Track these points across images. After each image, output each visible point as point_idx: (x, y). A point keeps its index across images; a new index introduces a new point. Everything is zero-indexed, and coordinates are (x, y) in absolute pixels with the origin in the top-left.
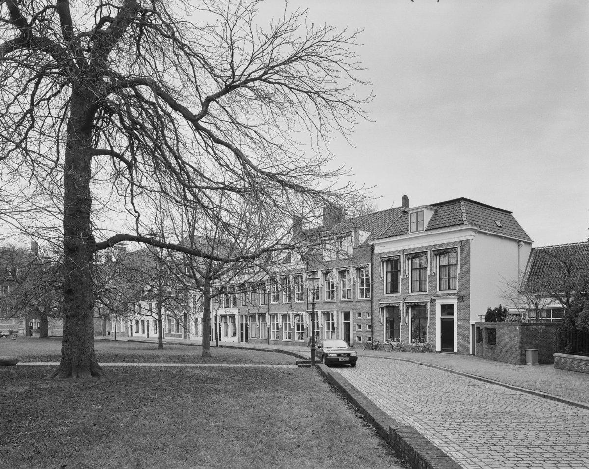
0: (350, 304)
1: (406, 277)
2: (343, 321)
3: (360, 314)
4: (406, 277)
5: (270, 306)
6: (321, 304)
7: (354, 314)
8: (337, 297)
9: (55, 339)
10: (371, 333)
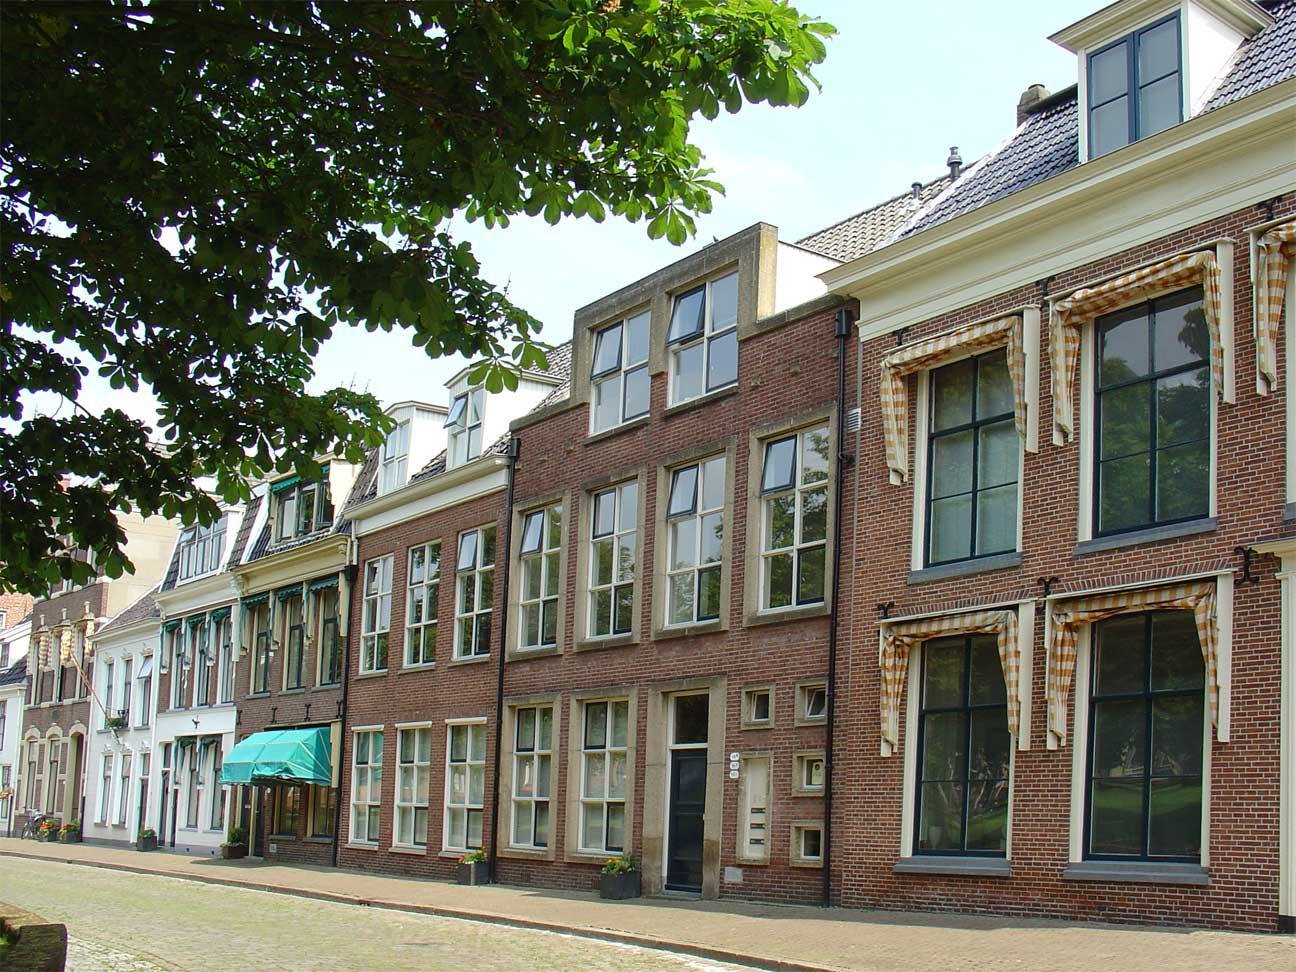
1: (1057, 440)
2: (671, 745)
3: (763, 701)
4: (1057, 440)
5: (352, 688)
6: (563, 662)
7: (733, 703)
8: (647, 617)
10: (821, 808)
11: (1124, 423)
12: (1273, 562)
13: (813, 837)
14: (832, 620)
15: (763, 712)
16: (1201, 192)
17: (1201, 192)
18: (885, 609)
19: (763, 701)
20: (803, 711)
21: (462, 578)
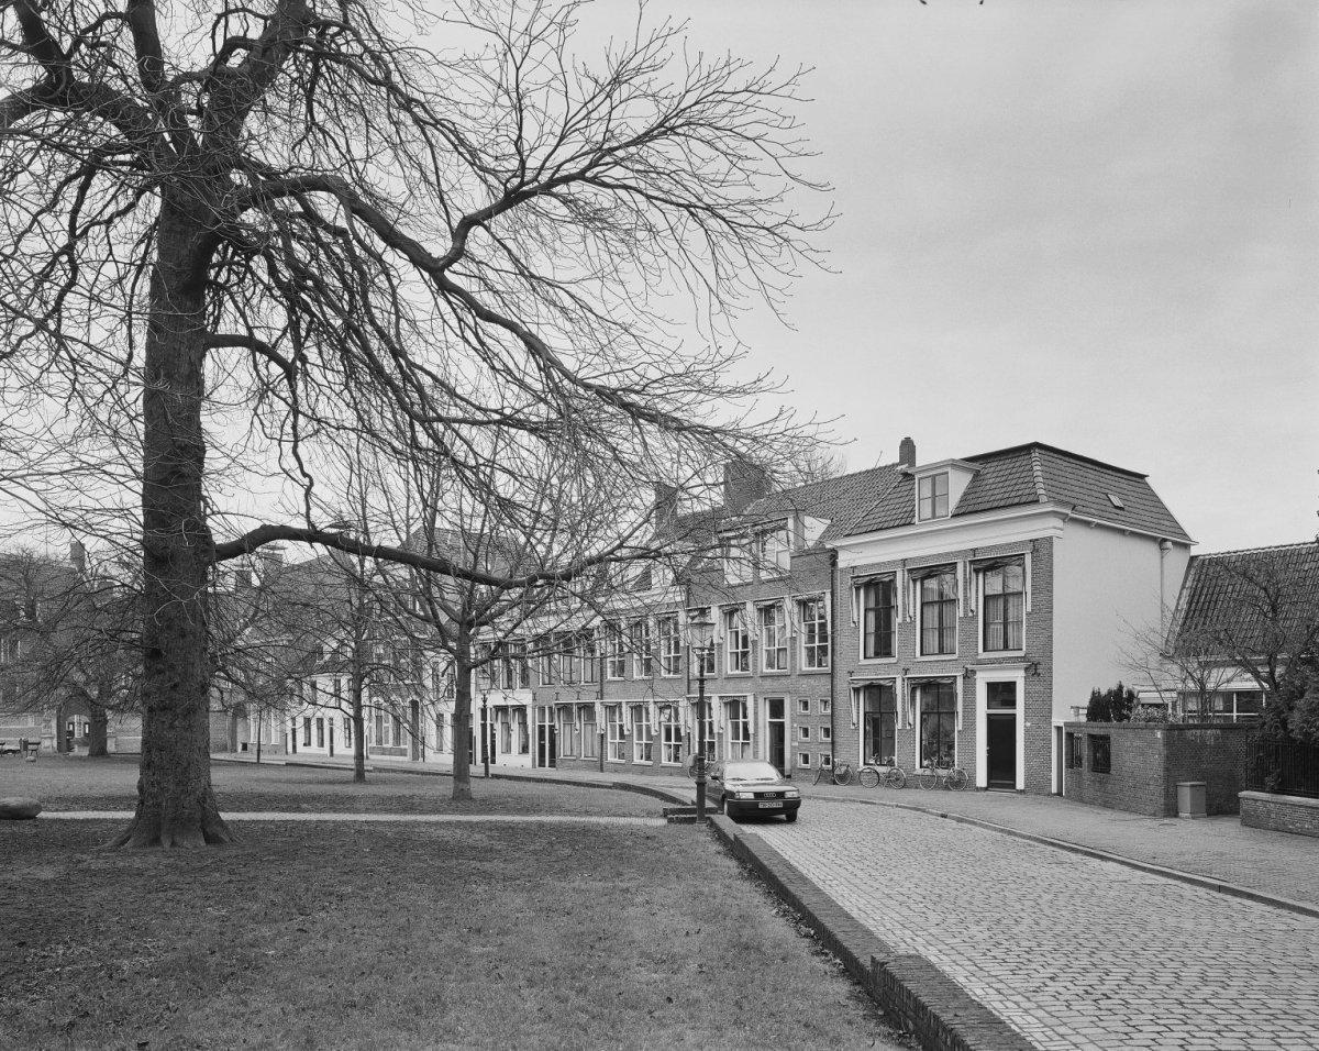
0: (783, 680)
1: (908, 620)
2: (768, 720)
3: (806, 705)
4: (908, 620)
5: (605, 686)
6: (718, 681)
7: (792, 704)
8: (755, 665)
9: (124, 759)
10: (830, 747)
11: (152, 295)
12: (974, 672)
13: (827, 730)
14: (832, 675)
15: (806, 761)
16: (882, 552)
17: (882, 552)
18: (851, 673)
19: (806, 705)
20: (821, 735)
21: (613, 662)
